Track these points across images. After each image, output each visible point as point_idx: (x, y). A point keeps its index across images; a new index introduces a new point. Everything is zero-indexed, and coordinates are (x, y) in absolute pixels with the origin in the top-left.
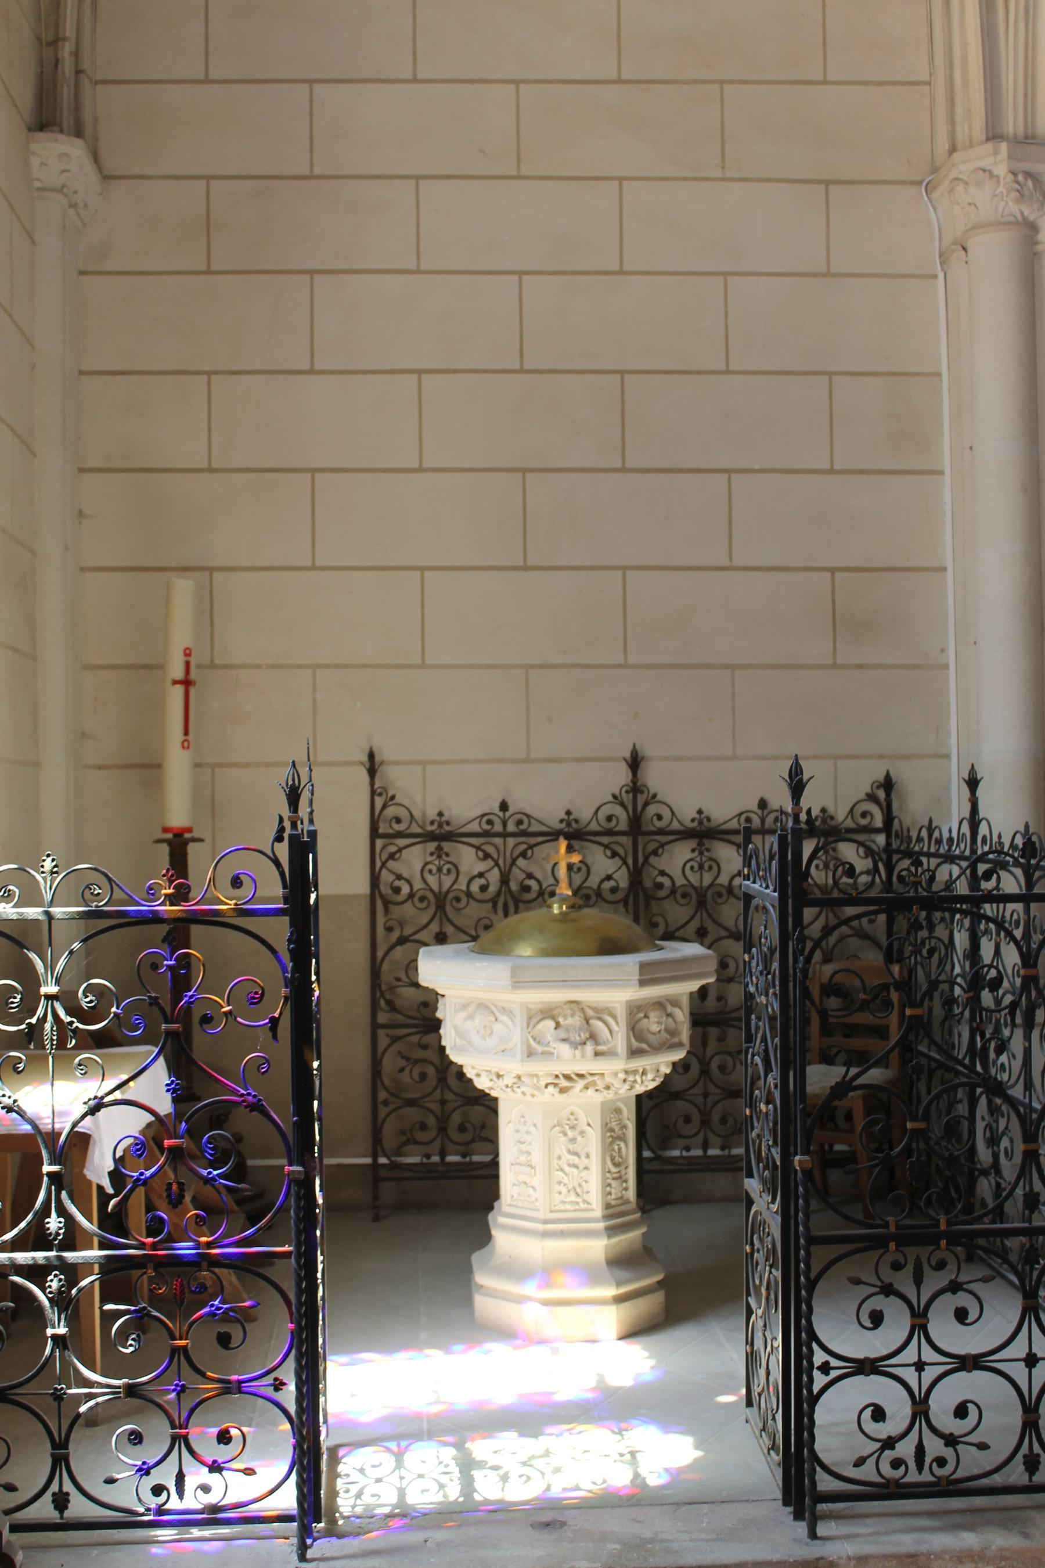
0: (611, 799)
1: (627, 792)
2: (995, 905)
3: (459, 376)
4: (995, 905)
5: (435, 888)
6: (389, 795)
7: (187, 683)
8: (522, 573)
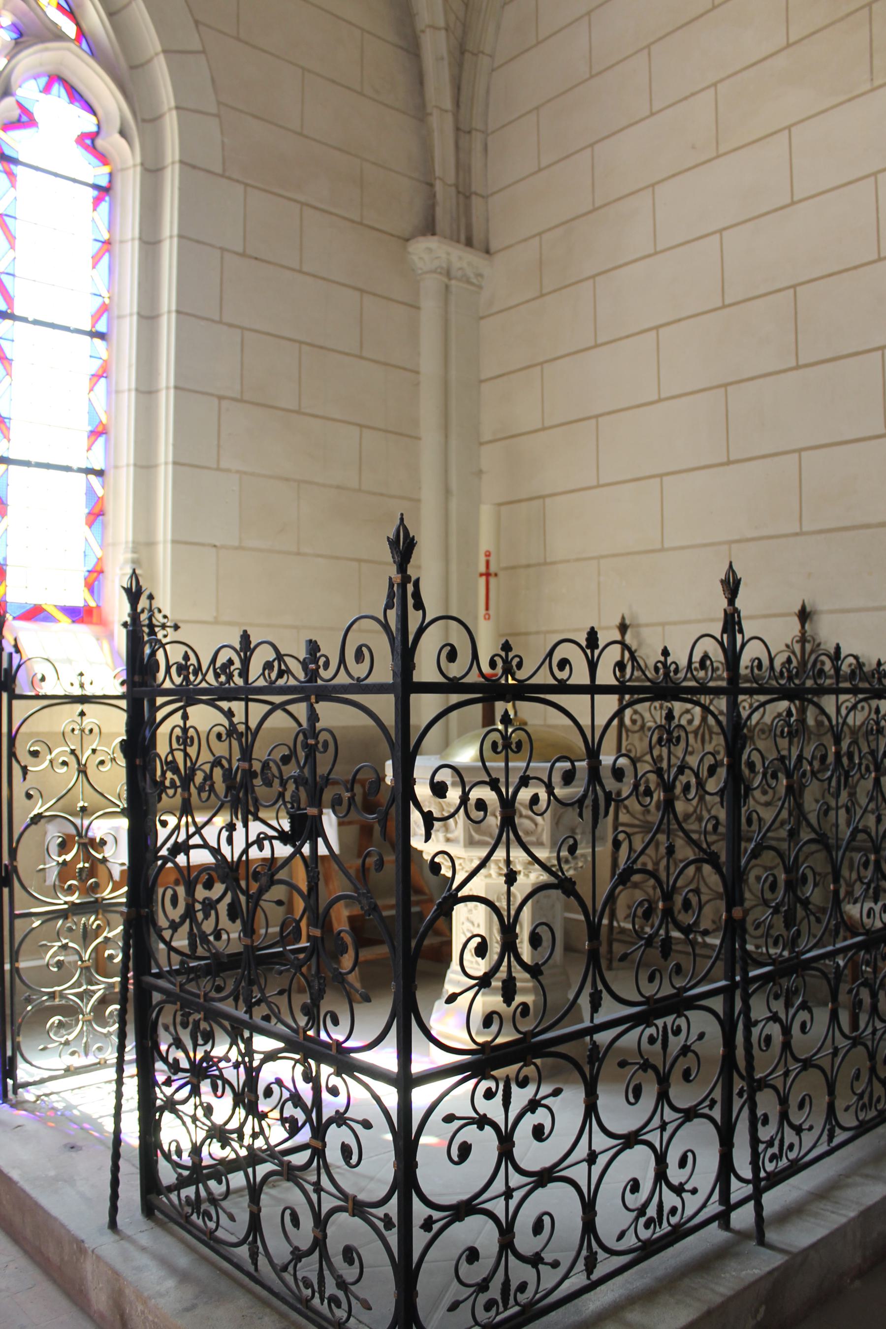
0: (784, 648)
1: (797, 642)
2: (124, 900)
3: (682, 323)
4: (124, 900)
5: (585, 721)
6: (816, 643)
7: (487, 575)
8: (726, 467)
